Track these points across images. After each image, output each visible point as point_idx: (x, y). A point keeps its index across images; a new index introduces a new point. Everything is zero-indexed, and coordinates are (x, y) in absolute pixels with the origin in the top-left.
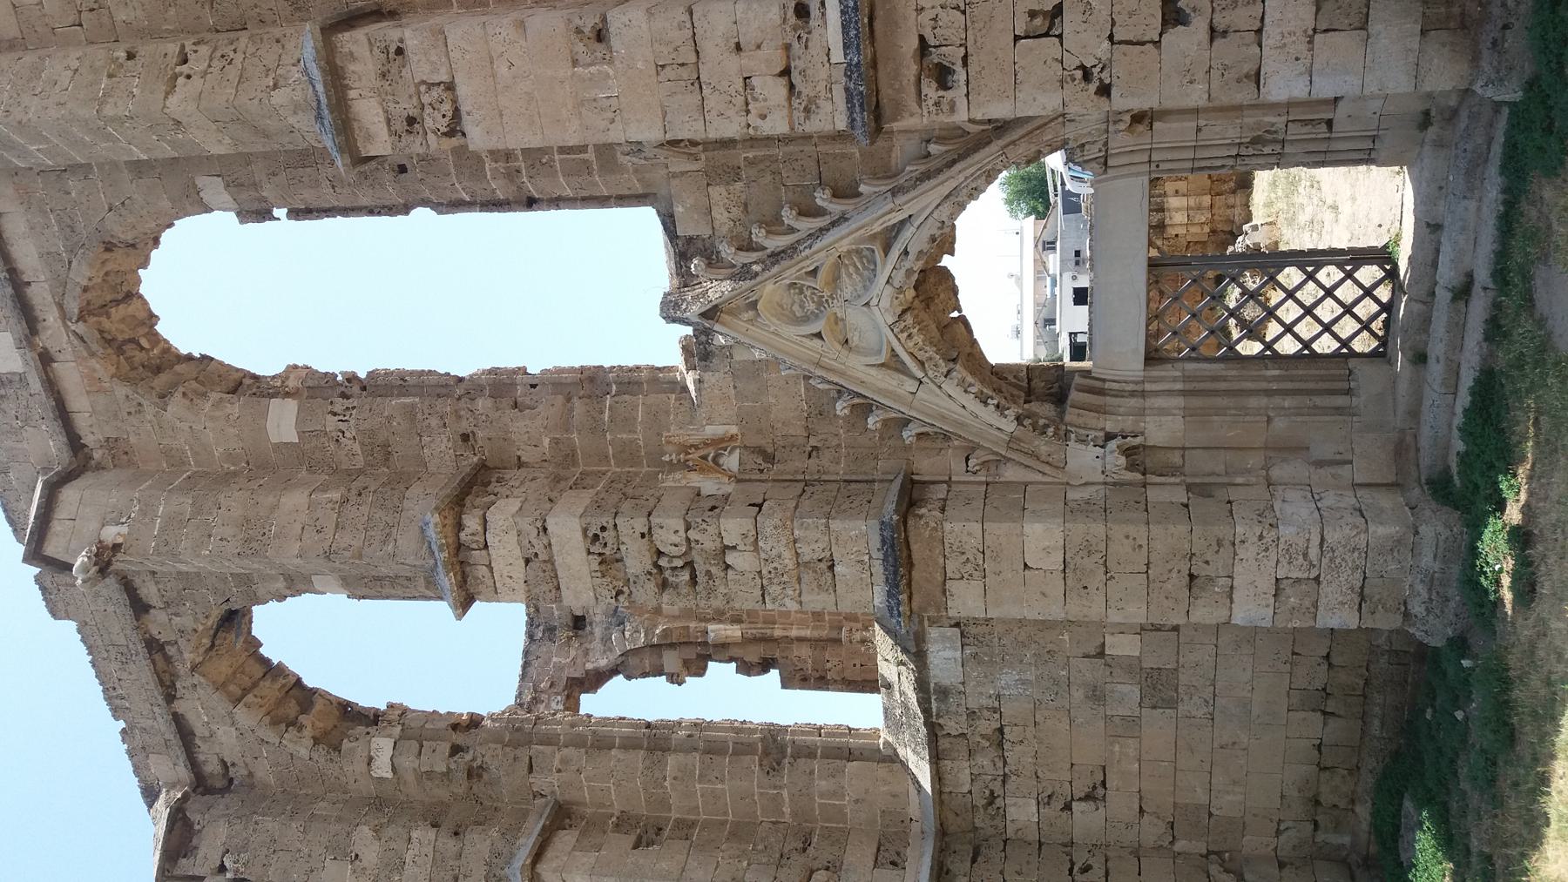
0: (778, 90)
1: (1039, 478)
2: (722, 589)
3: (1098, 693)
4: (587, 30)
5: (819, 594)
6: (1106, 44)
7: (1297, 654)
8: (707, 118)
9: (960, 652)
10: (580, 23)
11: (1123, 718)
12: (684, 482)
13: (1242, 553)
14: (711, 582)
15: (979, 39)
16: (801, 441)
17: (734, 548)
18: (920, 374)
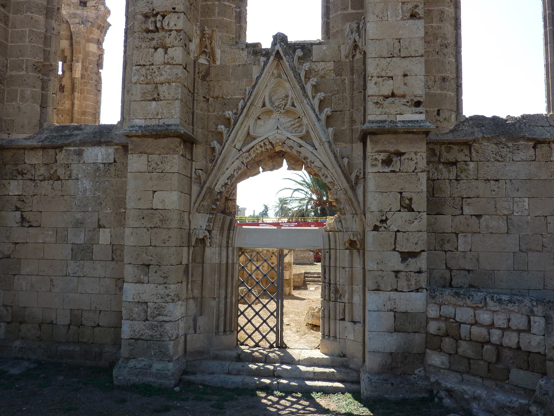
0: (387, 91)
1: (193, 201)
2: (144, 45)
3: (80, 225)
4: (417, 10)
5: (141, 93)
6: (396, 229)
7: (100, 313)
8: (377, 59)
9: (101, 162)
10: (420, 8)
11: (67, 236)
12: (195, 35)
13: (160, 287)
14: (148, 40)
15: (402, 177)
16: (212, 94)
17: (166, 53)
18: (244, 150)
